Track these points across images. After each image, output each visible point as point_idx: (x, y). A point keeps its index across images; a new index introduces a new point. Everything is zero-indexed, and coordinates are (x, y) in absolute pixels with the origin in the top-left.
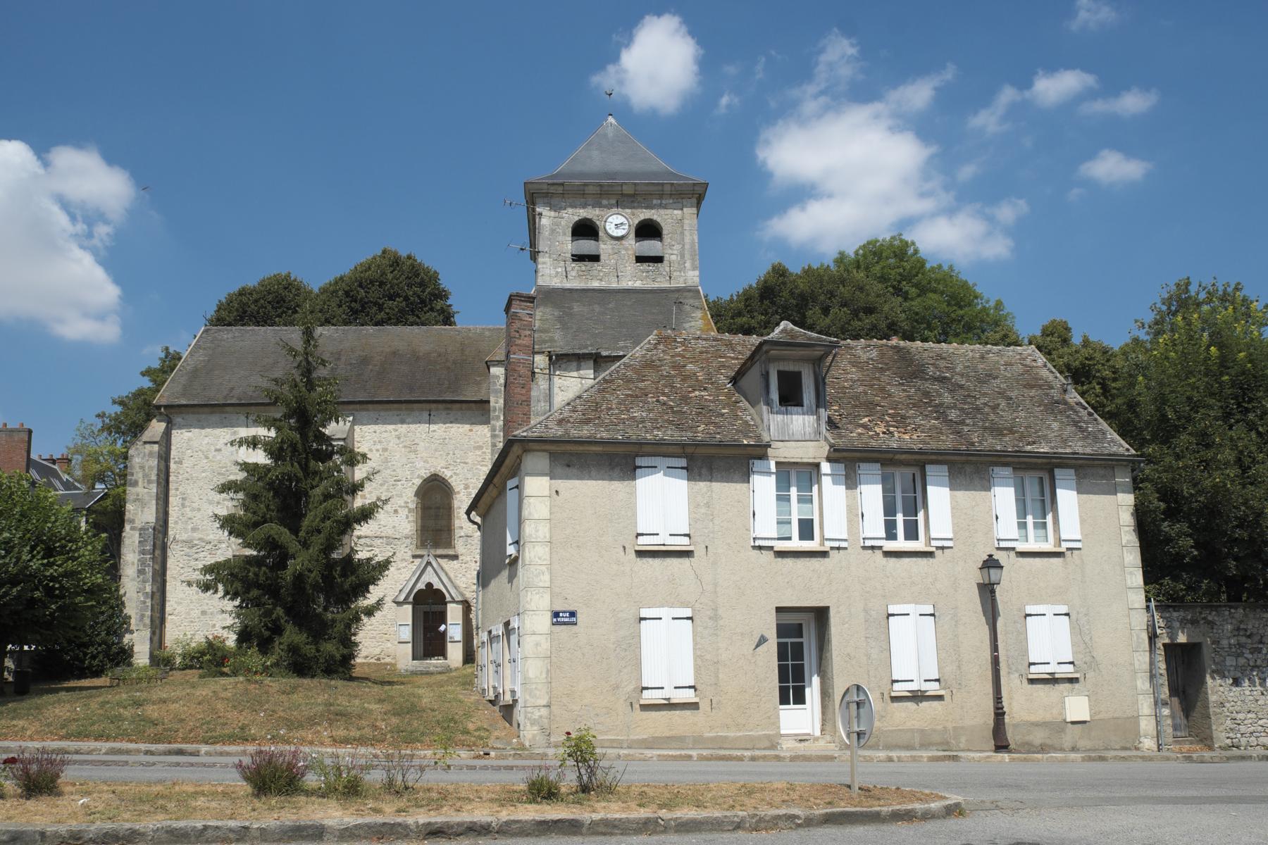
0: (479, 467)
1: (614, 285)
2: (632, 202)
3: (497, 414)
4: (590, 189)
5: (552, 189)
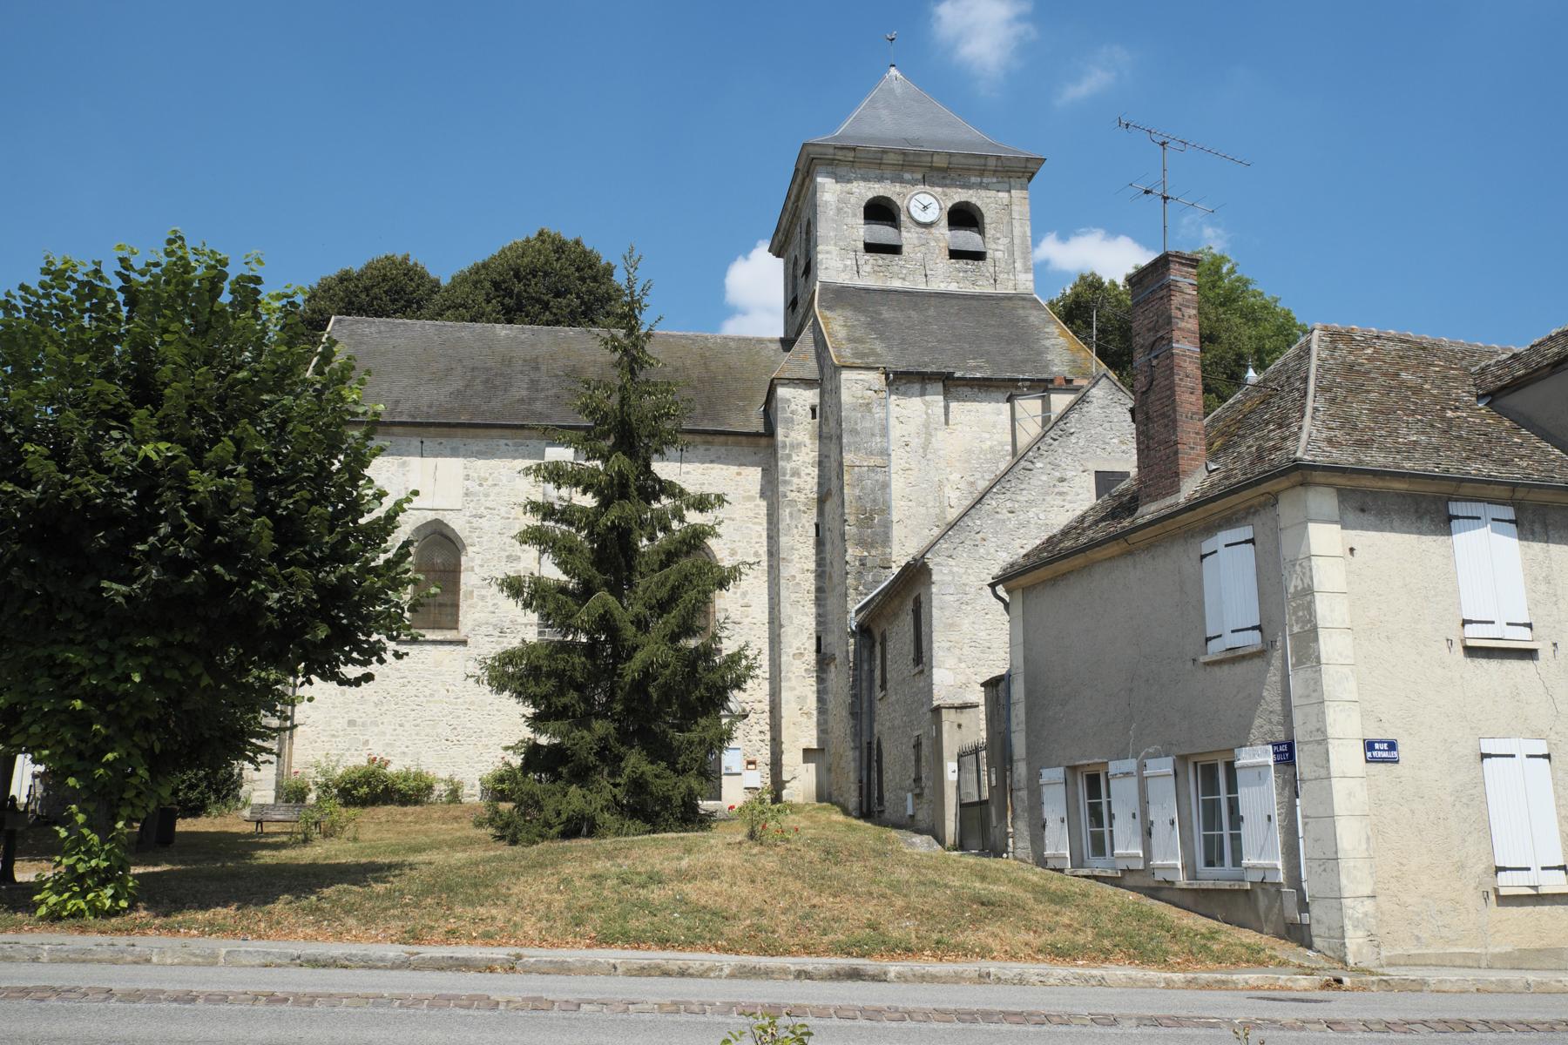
0: (750, 525)
1: (922, 287)
2: (944, 178)
3: (787, 452)
4: (890, 159)
5: (840, 155)
